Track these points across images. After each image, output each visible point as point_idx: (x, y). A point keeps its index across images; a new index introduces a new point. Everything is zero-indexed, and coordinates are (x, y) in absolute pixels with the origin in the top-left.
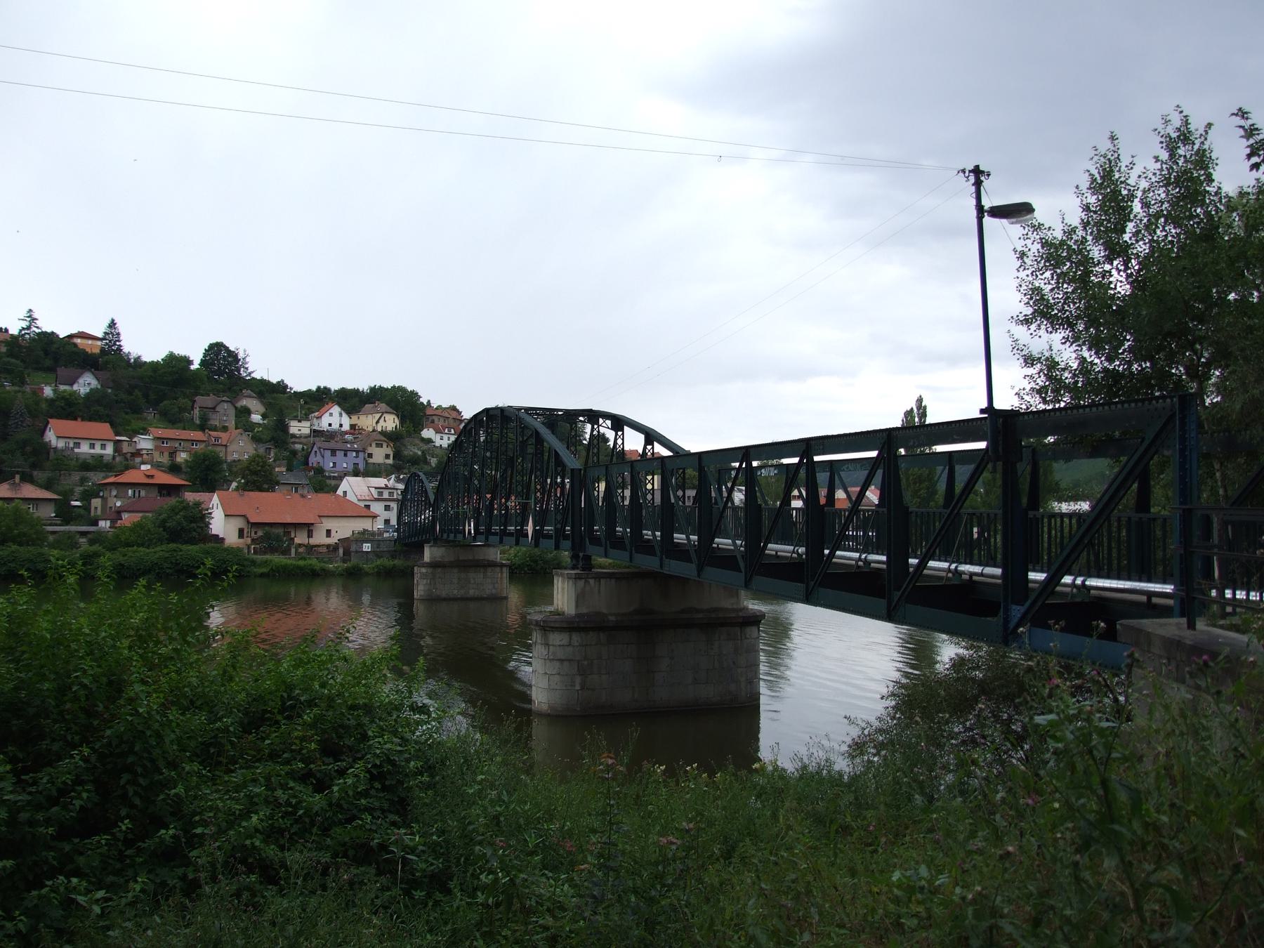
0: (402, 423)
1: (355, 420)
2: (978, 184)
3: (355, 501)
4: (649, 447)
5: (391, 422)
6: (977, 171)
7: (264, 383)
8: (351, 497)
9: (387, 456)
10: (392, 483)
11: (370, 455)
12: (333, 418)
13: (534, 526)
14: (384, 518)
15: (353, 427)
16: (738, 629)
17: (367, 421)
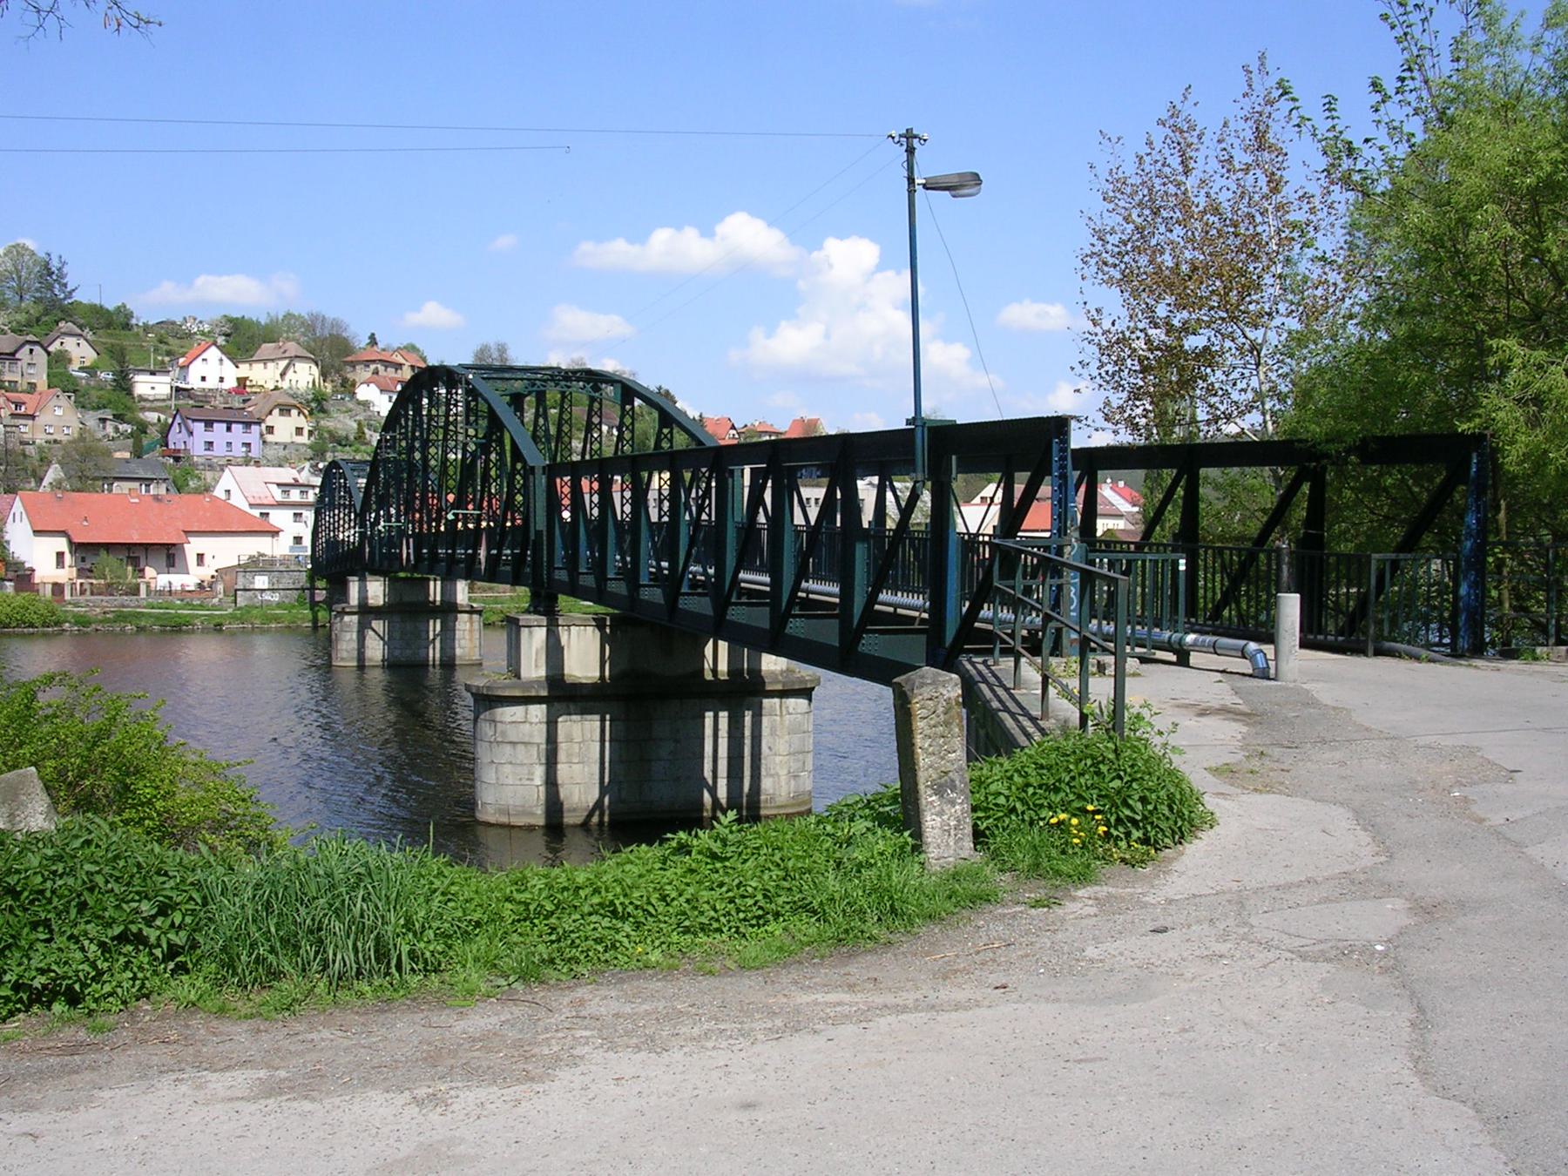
0: (324, 375)
1: (244, 370)
2: (910, 151)
3: (245, 507)
4: (666, 431)
5: (304, 376)
6: (909, 136)
7: (97, 311)
8: (238, 501)
9: (299, 431)
10: (304, 477)
11: (270, 429)
12: (211, 371)
13: (488, 550)
14: (293, 534)
15: (242, 382)
16: (777, 700)
17: (263, 375)
